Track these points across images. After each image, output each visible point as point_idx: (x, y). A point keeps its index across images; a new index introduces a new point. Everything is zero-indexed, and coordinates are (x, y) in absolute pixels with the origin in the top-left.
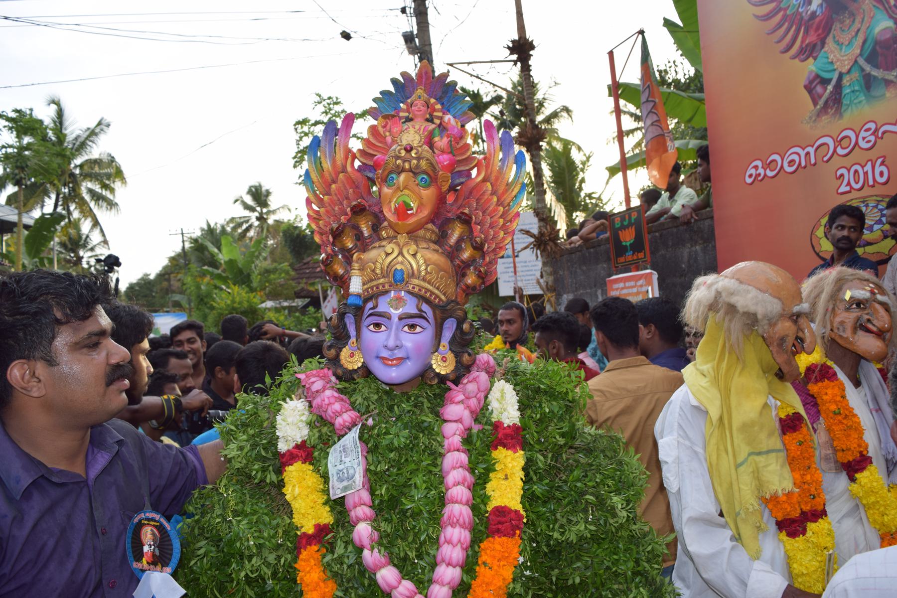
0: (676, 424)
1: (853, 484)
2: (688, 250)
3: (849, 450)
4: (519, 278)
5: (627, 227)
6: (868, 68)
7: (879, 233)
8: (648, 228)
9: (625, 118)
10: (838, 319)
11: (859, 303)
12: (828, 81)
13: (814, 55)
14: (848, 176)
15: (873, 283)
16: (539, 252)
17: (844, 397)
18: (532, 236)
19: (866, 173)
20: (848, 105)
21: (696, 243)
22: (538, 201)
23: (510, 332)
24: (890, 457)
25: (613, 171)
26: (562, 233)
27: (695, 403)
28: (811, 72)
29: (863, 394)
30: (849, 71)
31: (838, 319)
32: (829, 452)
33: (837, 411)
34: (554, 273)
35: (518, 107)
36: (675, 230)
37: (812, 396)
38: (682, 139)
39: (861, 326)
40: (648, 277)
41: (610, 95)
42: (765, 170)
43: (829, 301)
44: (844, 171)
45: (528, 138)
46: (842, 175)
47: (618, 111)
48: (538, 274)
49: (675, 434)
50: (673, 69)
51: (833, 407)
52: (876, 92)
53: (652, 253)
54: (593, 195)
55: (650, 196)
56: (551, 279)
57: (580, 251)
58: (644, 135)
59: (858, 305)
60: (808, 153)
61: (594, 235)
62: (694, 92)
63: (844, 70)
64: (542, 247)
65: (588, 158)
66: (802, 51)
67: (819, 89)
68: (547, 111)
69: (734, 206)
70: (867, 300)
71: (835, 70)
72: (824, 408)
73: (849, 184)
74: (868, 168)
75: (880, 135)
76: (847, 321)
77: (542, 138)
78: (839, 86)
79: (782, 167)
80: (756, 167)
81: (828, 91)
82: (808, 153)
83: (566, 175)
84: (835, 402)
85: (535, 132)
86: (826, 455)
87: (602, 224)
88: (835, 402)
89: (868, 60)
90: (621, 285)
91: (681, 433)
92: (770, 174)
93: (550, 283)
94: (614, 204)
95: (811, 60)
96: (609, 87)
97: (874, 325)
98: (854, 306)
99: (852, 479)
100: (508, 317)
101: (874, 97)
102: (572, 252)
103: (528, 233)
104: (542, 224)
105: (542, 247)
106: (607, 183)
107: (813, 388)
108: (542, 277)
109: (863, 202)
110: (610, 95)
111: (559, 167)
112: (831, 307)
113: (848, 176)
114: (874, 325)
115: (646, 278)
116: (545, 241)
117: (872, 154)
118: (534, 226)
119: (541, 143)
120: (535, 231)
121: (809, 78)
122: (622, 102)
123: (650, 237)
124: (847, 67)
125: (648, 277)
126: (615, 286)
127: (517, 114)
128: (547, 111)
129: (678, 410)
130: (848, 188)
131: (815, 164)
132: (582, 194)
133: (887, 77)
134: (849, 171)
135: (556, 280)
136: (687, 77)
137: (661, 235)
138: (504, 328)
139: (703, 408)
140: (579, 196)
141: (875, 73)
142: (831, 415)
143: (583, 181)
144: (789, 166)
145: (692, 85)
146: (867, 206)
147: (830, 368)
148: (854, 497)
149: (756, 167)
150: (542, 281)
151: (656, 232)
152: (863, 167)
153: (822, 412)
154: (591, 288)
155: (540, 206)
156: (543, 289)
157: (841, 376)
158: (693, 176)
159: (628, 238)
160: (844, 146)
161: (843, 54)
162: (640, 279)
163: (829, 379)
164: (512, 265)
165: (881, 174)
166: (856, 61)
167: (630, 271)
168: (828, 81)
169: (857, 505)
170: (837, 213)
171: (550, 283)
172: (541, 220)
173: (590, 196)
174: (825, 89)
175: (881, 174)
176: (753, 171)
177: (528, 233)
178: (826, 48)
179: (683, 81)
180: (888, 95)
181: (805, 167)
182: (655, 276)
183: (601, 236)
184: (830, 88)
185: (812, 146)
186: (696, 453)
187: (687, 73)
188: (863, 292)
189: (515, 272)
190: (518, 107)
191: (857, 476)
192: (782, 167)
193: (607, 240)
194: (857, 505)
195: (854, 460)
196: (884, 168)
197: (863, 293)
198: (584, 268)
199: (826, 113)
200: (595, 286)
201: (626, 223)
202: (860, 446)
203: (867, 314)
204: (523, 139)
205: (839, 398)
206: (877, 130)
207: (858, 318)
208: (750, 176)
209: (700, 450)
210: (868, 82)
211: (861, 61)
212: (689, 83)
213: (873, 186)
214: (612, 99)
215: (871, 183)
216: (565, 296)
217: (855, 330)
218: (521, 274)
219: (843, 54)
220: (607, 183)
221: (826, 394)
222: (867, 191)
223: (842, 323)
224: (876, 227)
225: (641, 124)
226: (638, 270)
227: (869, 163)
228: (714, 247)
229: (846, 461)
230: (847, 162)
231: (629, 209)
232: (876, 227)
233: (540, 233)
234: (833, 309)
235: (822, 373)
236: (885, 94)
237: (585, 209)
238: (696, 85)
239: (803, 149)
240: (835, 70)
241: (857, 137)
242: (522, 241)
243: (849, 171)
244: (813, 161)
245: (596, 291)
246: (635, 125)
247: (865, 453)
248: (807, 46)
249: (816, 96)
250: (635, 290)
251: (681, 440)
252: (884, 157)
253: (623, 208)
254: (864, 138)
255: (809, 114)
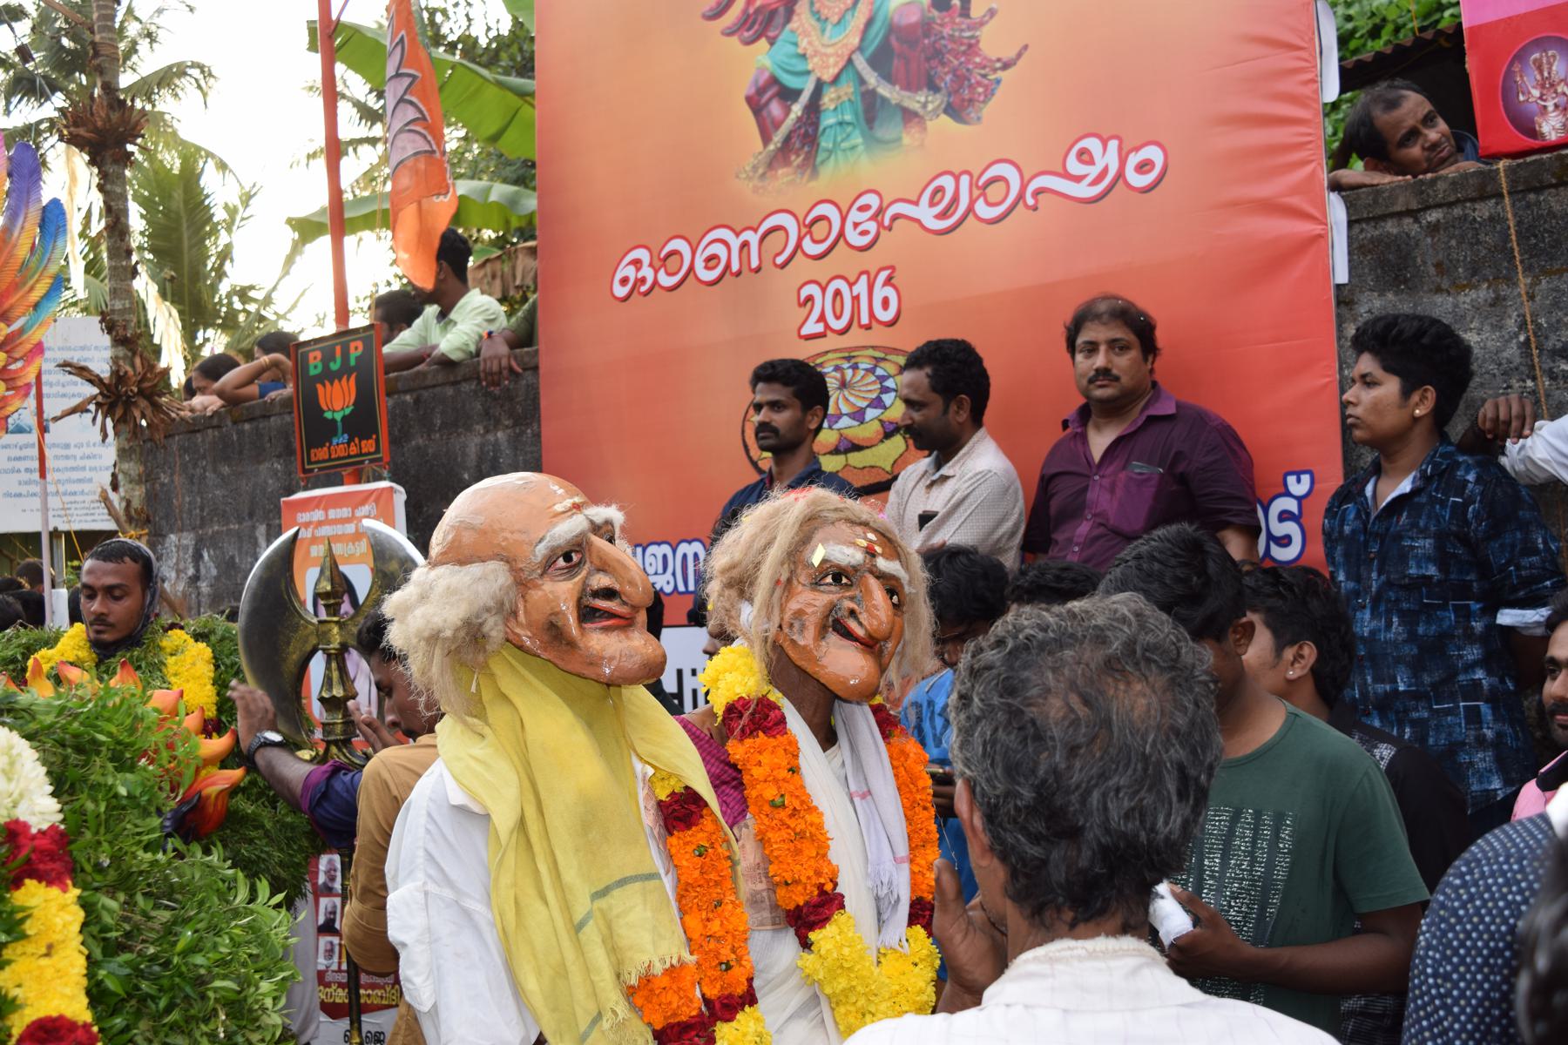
0: (421, 853)
1: (805, 955)
2: (477, 440)
3: (797, 882)
4: (51, 488)
5: (338, 375)
6: (872, 79)
7: (876, 426)
8: (387, 381)
9: (345, 111)
10: (794, 605)
11: (839, 575)
12: (794, 95)
13: (771, 34)
14: (823, 302)
15: (875, 531)
16: (109, 423)
17: (794, 770)
18: (94, 380)
19: (856, 299)
20: (830, 152)
21: (497, 423)
22: (114, 293)
23: (111, 619)
24: (883, 892)
25: (306, 229)
26: (177, 378)
27: (458, 798)
28: (761, 70)
29: (837, 761)
30: (835, 80)
31: (794, 605)
32: (761, 886)
33: (778, 800)
34: (147, 478)
35: (65, 42)
36: (450, 391)
37: (734, 766)
38: (472, 178)
39: (835, 624)
40: (383, 498)
41: (312, 47)
42: (656, 272)
43: (782, 564)
44: (813, 290)
45: (96, 130)
46: (810, 298)
47: (331, 95)
48: (107, 479)
49: (420, 875)
50: (462, 10)
51: (770, 792)
52: (884, 131)
53: (396, 441)
54: (252, 294)
55: (397, 310)
56: (138, 494)
57: (219, 427)
58: (385, 159)
59: (837, 578)
60: (745, 244)
61: (253, 389)
62: (507, 73)
63: (827, 76)
64: (119, 412)
65: (247, 199)
66: (746, 22)
67: (775, 109)
68: (147, 62)
69: (589, 348)
70: (855, 569)
71: (808, 73)
72: (754, 794)
73: (822, 318)
74: (861, 287)
75: (887, 222)
76: (809, 610)
77: (132, 135)
78: (814, 108)
79: (691, 268)
80: (637, 263)
81: (793, 116)
82: (745, 244)
83: (183, 236)
84: (776, 781)
85: (115, 116)
86: (754, 894)
87: (275, 364)
88: (776, 781)
89: (874, 62)
90: (318, 515)
91: (432, 872)
92: (666, 281)
93: (136, 504)
94: (306, 314)
95: (763, 42)
96: (312, 31)
97: (860, 624)
98: (829, 580)
99: (806, 945)
100: (110, 580)
101: (879, 141)
102: (198, 425)
103: (81, 371)
104: (121, 351)
105: (119, 412)
106: (290, 261)
107: (737, 750)
108: (115, 487)
109: (848, 359)
110: (312, 47)
111: (166, 214)
112: (784, 578)
113: (823, 302)
114: (860, 624)
115: (377, 501)
116: (128, 395)
117: (870, 260)
118: (100, 355)
119: (130, 148)
120: (103, 369)
121: (756, 81)
122: (340, 68)
123: (390, 402)
124: (833, 71)
125: (383, 498)
126: (303, 517)
127: (66, 63)
128: (147, 62)
129: (423, 820)
130: (820, 328)
131: (758, 270)
132: (224, 288)
133: (908, 103)
134: (824, 290)
135: (151, 497)
136: (492, 34)
137: (417, 401)
138: (96, 606)
139: (476, 809)
140: (214, 288)
141: (885, 90)
142: (767, 808)
143: (225, 255)
144: (707, 268)
145: (504, 55)
146: (855, 367)
147: (773, 706)
148: (809, 981)
149: (637, 263)
150: (113, 496)
151: (405, 392)
152: (851, 285)
153: (750, 802)
154: (240, 520)
155: (118, 305)
156: (117, 521)
157: (796, 724)
158: (489, 268)
159: (338, 402)
160: (817, 237)
161: (825, 40)
162: (363, 503)
163: (768, 731)
164: (35, 452)
165: (886, 303)
166: (850, 61)
167: (342, 484)
168: (794, 95)
169: (816, 997)
170: (768, 373)
171: (136, 504)
172: (119, 341)
173: (243, 294)
174: (788, 111)
175: (886, 303)
176: (630, 272)
177: (81, 371)
178: (794, 25)
179: (483, 42)
180: (906, 140)
181: (738, 274)
182: (400, 496)
183: (273, 394)
184: (797, 109)
185: (755, 230)
186: (467, 914)
187: (493, 25)
188: (849, 551)
189: (43, 475)
190: (65, 42)
191: (813, 936)
192: (691, 268)
193: (287, 403)
194: (816, 997)
195: (807, 903)
196: (890, 292)
197: (848, 555)
198: (226, 470)
199: (787, 162)
200: (251, 515)
201: (335, 366)
202: (818, 873)
203: (852, 599)
204: (82, 131)
205: (784, 774)
206: (881, 210)
207: (832, 607)
208: (624, 281)
209: (477, 907)
210: (871, 109)
211: (860, 62)
212: (497, 50)
213: (868, 327)
214: (317, 58)
215: (865, 320)
216: (173, 537)
217: (822, 632)
218: (57, 476)
219: (825, 40)
220: (290, 261)
221: (759, 764)
222: (855, 338)
223: (799, 614)
224: (871, 413)
225: (378, 130)
226: (359, 482)
227: (864, 278)
228: (538, 436)
229: (792, 907)
230: (821, 270)
231: (345, 334)
232: (871, 413)
233: (115, 373)
234: (789, 581)
235: (755, 718)
236: (899, 139)
237: (229, 323)
238: (512, 58)
239: (737, 234)
240: (808, 73)
241: (844, 220)
242: (66, 391)
243: (824, 290)
244: (755, 263)
245: (254, 528)
246: (363, 131)
247: (828, 887)
248: (758, 11)
249: (768, 121)
250: (350, 528)
251: (431, 887)
252: (893, 268)
253: (331, 328)
254: (856, 225)
255: (752, 161)
